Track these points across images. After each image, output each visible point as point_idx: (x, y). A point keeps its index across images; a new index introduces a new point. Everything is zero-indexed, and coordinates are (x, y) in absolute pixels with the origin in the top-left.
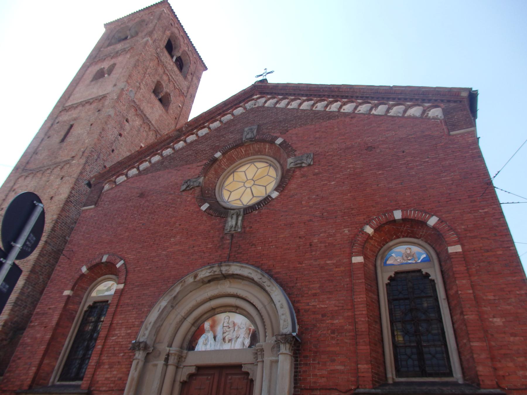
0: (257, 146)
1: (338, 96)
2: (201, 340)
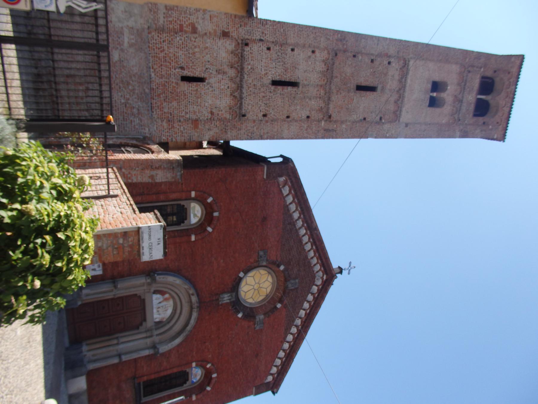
1: (276, 381)
2: (158, 296)
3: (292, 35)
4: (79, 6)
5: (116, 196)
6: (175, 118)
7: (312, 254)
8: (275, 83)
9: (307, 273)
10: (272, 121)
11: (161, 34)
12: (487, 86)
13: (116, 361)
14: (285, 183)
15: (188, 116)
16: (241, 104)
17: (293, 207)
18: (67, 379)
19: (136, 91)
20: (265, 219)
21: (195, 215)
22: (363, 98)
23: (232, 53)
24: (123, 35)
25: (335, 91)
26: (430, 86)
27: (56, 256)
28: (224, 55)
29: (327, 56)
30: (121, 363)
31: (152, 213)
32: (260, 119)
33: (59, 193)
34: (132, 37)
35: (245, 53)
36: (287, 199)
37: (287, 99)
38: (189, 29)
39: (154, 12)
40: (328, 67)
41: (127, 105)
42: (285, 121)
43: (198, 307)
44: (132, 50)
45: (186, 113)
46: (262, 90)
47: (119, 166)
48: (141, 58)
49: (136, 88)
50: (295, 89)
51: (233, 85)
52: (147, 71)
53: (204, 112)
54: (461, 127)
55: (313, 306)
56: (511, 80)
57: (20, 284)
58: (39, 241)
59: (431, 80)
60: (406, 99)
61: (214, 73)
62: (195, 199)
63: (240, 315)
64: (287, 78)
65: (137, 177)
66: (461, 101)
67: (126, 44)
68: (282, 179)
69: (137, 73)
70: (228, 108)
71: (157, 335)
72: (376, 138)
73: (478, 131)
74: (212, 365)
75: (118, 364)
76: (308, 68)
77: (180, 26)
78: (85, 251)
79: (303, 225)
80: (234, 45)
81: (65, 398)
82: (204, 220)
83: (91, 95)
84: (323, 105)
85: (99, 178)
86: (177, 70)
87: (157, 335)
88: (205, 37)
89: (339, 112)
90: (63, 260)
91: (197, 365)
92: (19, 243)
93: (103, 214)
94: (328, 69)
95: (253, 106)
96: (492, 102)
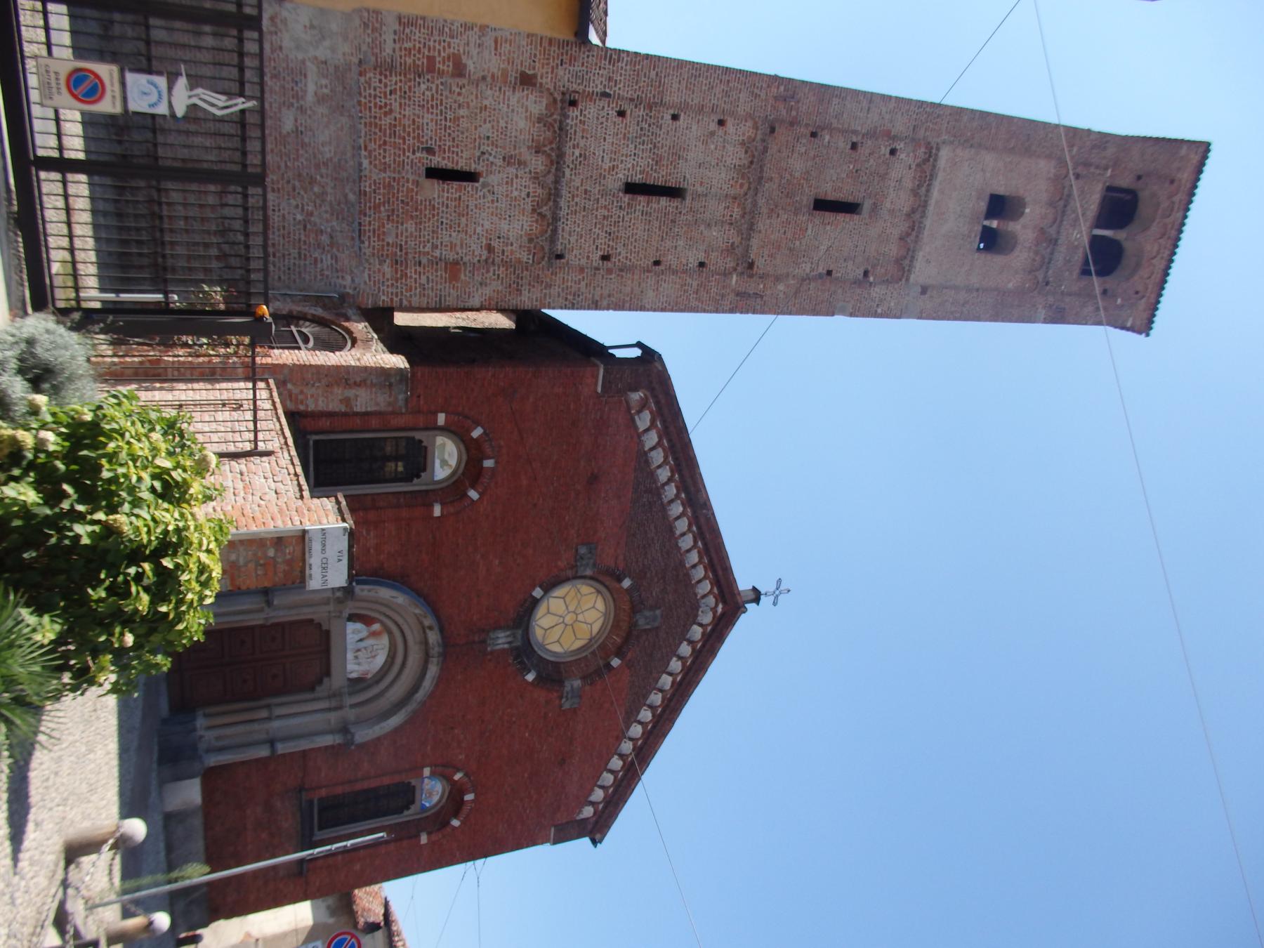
0: (624, 626)
1: (600, 817)
2: (359, 626)
3: (675, 86)
4: (213, 105)
5: (268, 454)
6: (410, 256)
7: (694, 557)
8: (632, 188)
9: (680, 599)
10: (621, 270)
11: (386, 77)
12: (1120, 208)
13: (264, 752)
14: (643, 405)
15: (437, 253)
16: (555, 231)
17: (657, 457)
18: (162, 783)
19: (329, 198)
20: (594, 479)
21: (444, 463)
22: (828, 228)
23: (540, 120)
24: (305, 76)
25: (765, 210)
26: (983, 206)
27: (158, 595)
28: (522, 124)
29: (751, 133)
30: (274, 757)
31: (333, 499)
32: (595, 264)
33: (166, 485)
34: (324, 82)
35: (569, 121)
36: (644, 438)
37: (657, 224)
38: (448, 67)
39: (374, 30)
40: (753, 156)
41: (309, 226)
42: (649, 271)
43: (440, 655)
44: (322, 110)
45: (435, 247)
46: (602, 201)
47: (281, 377)
48: (342, 129)
49: (329, 190)
50: (676, 203)
51: (539, 191)
52: (354, 156)
53: (474, 247)
54: (1051, 299)
55: (690, 668)
56: (1176, 199)
57: (102, 639)
58: (132, 571)
59: (989, 191)
60: (926, 232)
61: (499, 162)
62: (446, 430)
63: (530, 677)
64: (658, 177)
65: (317, 400)
66: (1054, 242)
67: (310, 97)
68: (636, 396)
69: (331, 159)
70: (525, 239)
71: (353, 706)
72: (851, 315)
73: (1089, 309)
74: (466, 775)
75: (266, 758)
76: (708, 159)
77: (426, 59)
78: (205, 585)
79: (677, 496)
80: (544, 104)
81: (158, 818)
82: (463, 474)
83: (231, 202)
84: (737, 240)
85: (239, 407)
86: (418, 155)
87: (353, 706)
88: (482, 86)
89: (771, 256)
90: (170, 602)
91: (433, 774)
92: (103, 576)
93: (242, 494)
94: (752, 163)
95: (580, 237)
96: (1128, 246)
